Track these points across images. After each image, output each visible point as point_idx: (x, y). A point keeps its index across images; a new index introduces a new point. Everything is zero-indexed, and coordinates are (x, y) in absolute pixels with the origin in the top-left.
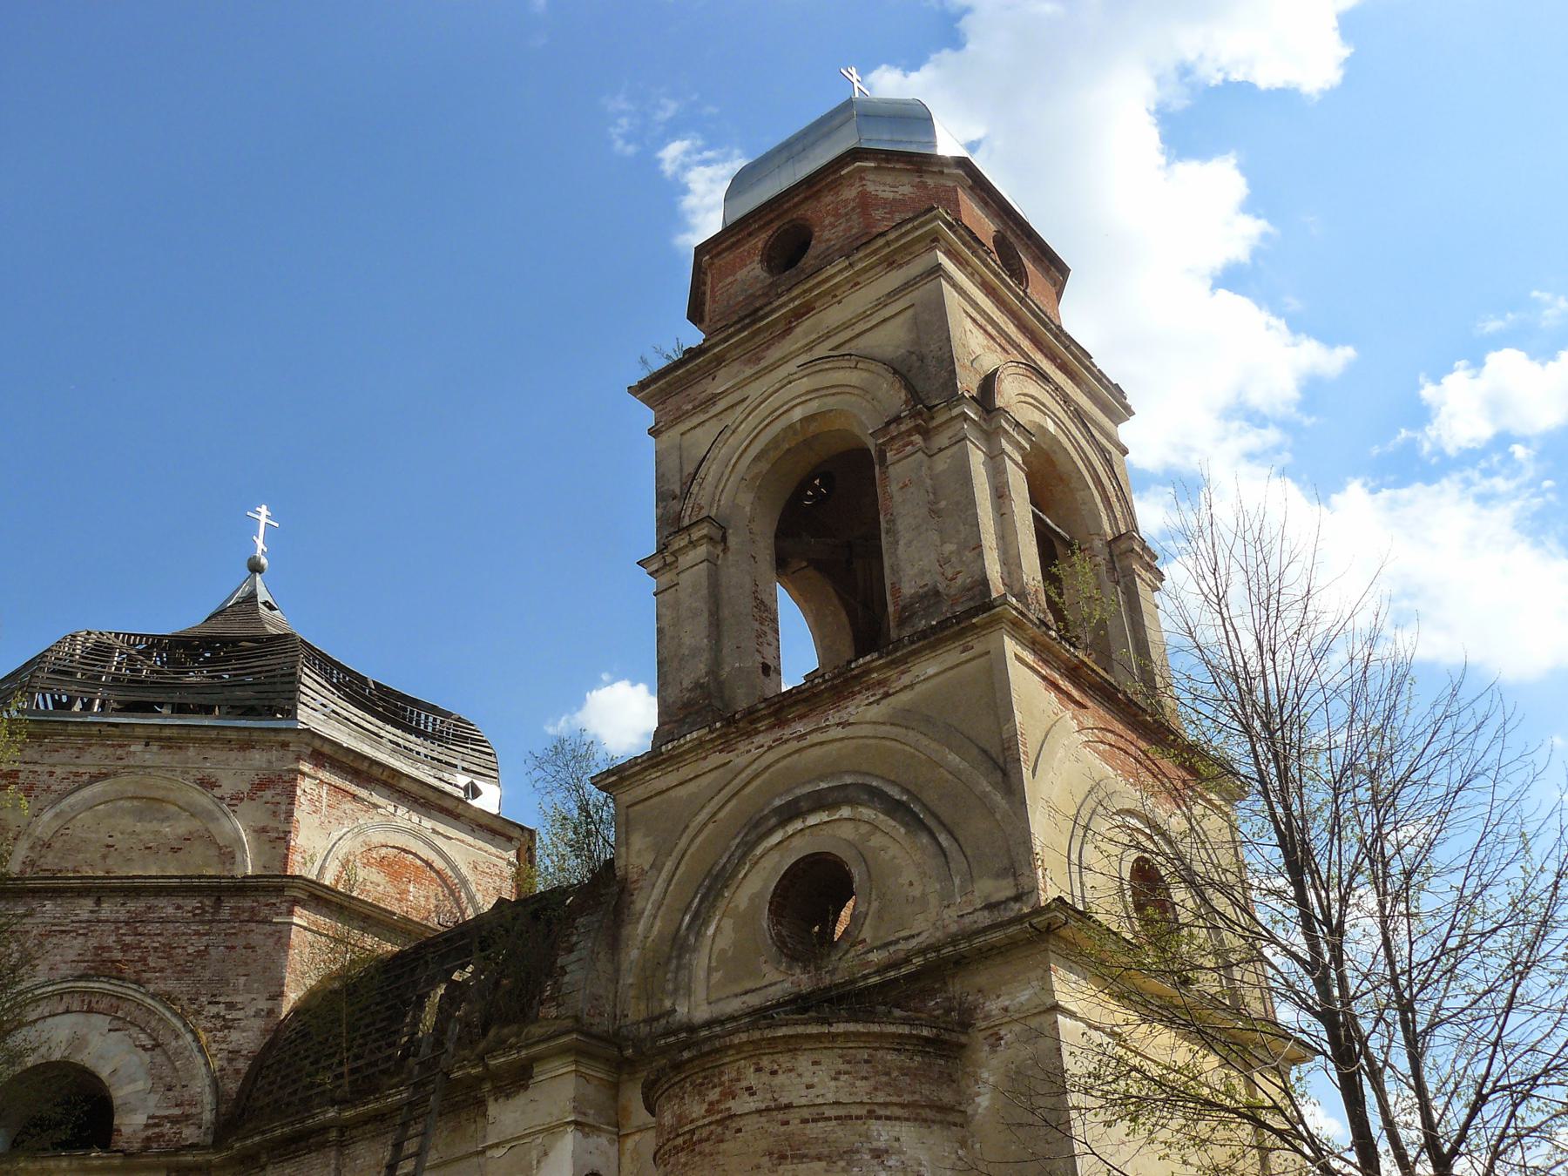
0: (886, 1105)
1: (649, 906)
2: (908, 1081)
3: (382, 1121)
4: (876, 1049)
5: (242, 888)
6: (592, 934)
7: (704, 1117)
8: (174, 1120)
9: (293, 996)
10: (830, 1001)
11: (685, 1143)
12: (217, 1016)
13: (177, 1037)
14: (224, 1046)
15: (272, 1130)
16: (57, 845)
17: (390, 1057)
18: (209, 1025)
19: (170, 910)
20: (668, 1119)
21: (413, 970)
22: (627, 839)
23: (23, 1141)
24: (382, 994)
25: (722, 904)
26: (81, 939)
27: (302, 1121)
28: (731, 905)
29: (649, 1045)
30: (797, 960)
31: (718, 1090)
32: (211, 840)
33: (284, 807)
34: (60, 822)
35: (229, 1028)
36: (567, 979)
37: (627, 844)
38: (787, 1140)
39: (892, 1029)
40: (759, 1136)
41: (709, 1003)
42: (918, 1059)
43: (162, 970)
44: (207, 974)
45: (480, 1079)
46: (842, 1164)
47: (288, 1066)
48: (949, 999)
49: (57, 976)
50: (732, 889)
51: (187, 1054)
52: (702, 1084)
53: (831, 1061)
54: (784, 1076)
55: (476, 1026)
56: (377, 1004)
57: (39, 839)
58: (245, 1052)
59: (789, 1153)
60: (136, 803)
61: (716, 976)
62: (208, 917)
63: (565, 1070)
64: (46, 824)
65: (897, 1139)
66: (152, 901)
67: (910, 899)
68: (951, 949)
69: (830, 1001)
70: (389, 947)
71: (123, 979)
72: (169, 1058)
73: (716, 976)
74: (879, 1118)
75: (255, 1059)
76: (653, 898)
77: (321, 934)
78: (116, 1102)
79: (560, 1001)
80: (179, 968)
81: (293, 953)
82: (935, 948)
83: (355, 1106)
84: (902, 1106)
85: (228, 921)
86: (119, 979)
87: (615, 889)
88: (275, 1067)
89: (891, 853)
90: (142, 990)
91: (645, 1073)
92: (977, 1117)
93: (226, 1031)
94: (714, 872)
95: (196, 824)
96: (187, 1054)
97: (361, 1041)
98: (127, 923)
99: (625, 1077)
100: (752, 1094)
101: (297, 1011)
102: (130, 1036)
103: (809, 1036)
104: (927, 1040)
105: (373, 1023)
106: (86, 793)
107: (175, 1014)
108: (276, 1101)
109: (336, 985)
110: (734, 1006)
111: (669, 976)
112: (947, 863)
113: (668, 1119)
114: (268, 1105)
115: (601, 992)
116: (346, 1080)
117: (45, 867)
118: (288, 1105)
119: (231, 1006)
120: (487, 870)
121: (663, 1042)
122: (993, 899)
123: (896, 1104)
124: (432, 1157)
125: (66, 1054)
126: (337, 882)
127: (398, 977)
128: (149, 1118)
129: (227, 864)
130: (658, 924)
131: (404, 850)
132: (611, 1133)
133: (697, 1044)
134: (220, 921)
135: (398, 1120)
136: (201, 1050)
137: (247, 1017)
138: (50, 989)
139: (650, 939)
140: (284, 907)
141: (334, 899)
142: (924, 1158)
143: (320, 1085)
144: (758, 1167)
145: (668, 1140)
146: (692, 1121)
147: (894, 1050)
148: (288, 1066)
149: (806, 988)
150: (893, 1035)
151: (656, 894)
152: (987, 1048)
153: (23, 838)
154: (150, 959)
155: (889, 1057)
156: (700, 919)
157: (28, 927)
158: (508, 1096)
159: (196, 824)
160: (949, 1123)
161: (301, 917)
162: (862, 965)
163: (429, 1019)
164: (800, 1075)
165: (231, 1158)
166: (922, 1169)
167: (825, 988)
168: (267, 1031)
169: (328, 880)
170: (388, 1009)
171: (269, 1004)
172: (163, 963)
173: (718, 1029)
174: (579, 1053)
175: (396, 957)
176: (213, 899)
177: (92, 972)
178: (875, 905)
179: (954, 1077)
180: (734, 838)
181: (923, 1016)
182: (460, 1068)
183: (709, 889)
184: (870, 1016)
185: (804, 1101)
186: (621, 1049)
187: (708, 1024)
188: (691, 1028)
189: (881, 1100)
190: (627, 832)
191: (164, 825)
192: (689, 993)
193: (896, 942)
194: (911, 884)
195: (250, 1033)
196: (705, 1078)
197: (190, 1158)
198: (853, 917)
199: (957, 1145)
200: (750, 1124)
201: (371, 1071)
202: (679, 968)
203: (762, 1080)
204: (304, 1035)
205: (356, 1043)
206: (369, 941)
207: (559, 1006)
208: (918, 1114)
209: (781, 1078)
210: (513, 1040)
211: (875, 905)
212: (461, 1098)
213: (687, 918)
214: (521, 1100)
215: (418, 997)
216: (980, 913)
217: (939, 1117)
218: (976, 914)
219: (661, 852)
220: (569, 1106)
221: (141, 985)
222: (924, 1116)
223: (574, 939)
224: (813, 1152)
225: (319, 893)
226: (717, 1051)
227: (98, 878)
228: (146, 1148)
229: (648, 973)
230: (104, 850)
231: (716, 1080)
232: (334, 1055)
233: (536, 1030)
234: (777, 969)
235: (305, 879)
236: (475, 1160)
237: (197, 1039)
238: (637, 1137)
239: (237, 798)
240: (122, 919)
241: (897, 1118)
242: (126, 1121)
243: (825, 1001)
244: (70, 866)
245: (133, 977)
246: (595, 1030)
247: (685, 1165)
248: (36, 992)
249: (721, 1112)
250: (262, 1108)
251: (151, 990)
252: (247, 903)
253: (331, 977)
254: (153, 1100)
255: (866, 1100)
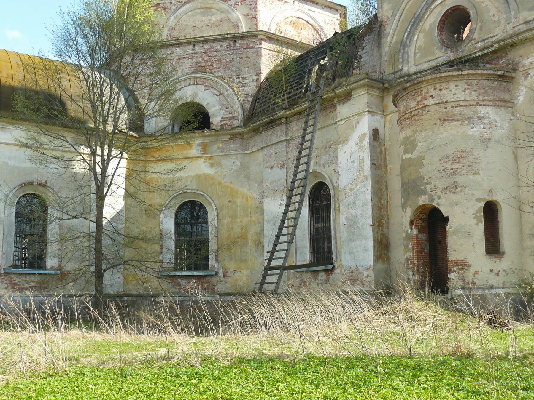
0: (483, 100)
1: (391, 31)
2: (492, 91)
3: (300, 114)
4: (480, 80)
5: (242, 37)
6: (371, 43)
7: (415, 107)
8: (230, 119)
9: (265, 73)
10: (462, 63)
11: (408, 116)
12: (240, 82)
13: (227, 90)
14: (243, 92)
15: (263, 120)
16: (177, 28)
17: (301, 92)
18: (237, 86)
19: (219, 47)
20: (402, 108)
21: (306, 61)
22: (382, 6)
23: (183, 128)
24: (296, 70)
25: (419, 28)
26: (190, 60)
27: (273, 116)
28: (423, 28)
29: (394, 82)
30: (449, 48)
31: (420, 97)
32: (229, 20)
33: (253, 6)
34: (177, 20)
35: (244, 86)
36: (362, 59)
37: (382, 8)
38: (446, 114)
39: (486, 72)
40: (436, 113)
41: (416, 66)
42: (496, 83)
43: (219, 68)
44: (234, 68)
45: (334, 98)
46: (467, 122)
47: (266, 98)
48: (508, 60)
49: (184, 73)
50: (423, 22)
51: (231, 96)
52: (414, 95)
53: (462, 85)
54: (445, 91)
55: (331, 79)
56: (295, 74)
57: (171, 27)
58: (251, 94)
59: (447, 119)
60: (201, 10)
61: (418, 55)
62: (232, 48)
63: (363, 93)
64: (172, 21)
65: (488, 113)
66: (212, 44)
67: (493, 22)
68: (510, 40)
69: (462, 63)
70: (297, 54)
71: (207, 73)
72: (225, 98)
73: (418, 55)
74: (480, 105)
75: (254, 96)
76: (393, 27)
77: (272, 51)
78: (210, 114)
79: (360, 68)
80: (225, 67)
81: (263, 58)
82: (504, 40)
83: (290, 110)
84: (490, 101)
85: (239, 49)
86: (205, 72)
87: (378, 25)
88: (261, 98)
89: (486, 3)
90: (213, 76)
91: (393, 92)
92: (518, 104)
93: (243, 87)
94: (416, 16)
95: (223, 16)
96: (231, 96)
97: (290, 87)
98: (205, 53)
99: (385, 94)
100: (433, 98)
101: (267, 79)
102: (211, 92)
103: (454, 76)
104: (500, 76)
105: (294, 81)
106: (184, 8)
107: (225, 83)
108: (263, 110)
109: (279, 68)
110: (425, 66)
111: (400, 56)
112: (509, 6)
113: (402, 108)
114: (260, 111)
115: (375, 64)
116: (286, 101)
117: (174, 36)
118: (267, 111)
119: (244, 79)
120: (329, 23)
121: (399, 81)
122: (527, 20)
123: (487, 100)
124: (318, 126)
125: (192, 99)
126: (276, 31)
127: (301, 64)
128: (221, 118)
129: (236, 28)
130: (395, 37)
131: (298, 18)
132: (381, 114)
133: (412, 80)
134: (236, 49)
135: (306, 114)
136: (235, 94)
137: (249, 82)
138: (183, 78)
139: (393, 43)
140: (258, 42)
141: (275, 38)
142: (498, 120)
143: (277, 103)
144: (436, 124)
145: (402, 116)
146: (411, 109)
147: (487, 80)
148: (266, 98)
149: (452, 59)
150: (487, 74)
151: (394, 26)
152: (523, 78)
153: (165, 27)
154: (214, 64)
155: (484, 83)
156: (411, 34)
157: (172, 58)
158: (343, 103)
159: (223, 16)
160: (507, 107)
161: (264, 45)
162: (474, 48)
163: (313, 77)
164: (451, 90)
165: (250, 130)
166: (497, 124)
167: (460, 58)
168: (257, 86)
169: (272, 31)
170: (298, 75)
171: (257, 77)
172: (219, 66)
173: (419, 75)
174: (369, 86)
175: (299, 57)
176: (233, 41)
177: (196, 71)
178: (479, 25)
179: (510, 90)
180: (423, 2)
181: (498, 66)
182: (326, 94)
183: (414, 22)
184: (477, 67)
185: (452, 100)
186: (383, 84)
187: (416, 73)
188: (409, 75)
189: (482, 99)
190: (381, 3)
191: (212, 17)
192: (408, 62)
193: (488, 39)
194: (494, 15)
195: (251, 87)
196: (415, 93)
197: (236, 131)
198: (471, 30)
199: (510, 115)
200: (432, 109)
201: (294, 97)
202: (403, 53)
203: (437, 93)
204: (270, 86)
205: (288, 88)
206: (289, 51)
207: (360, 70)
208: (495, 103)
209: (444, 91)
210: (344, 83)
211: (479, 25)
212: (328, 104)
213: (406, 34)
214: (348, 104)
215: (309, 70)
216: (522, 25)
217: (504, 104)
218: (521, 26)
219: (395, 10)
220: (366, 106)
221: (212, 74)
222: (498, 104)
223: (364, 45)
224: (456, 118)
225: (270, 36)
226: (419, 83)
227: (192, 38)
228: (222, 128)
229: (392, 56)
230: (193, 28)
231: (419, 93)
232: (281, 93)
233: (352, 79)
234: (441, 51)
235: (264, 31)
236: (333, 126)
237: (234, 91)
238: (391, 115)
239: (236, 4)
240: (203, 52)
241: (488, 105)
242: (214, 120)
243: (460, 63)
244: (183, 35)
245: (210, 71)
246: (373, 78)
247: (409, 124)
248: (179, 79)
249: (421, 105)
250: (258, 113)
251: (216, 75)
252: (245, 42)
253: (277, 66)
254: (222, 112)
255: (476, 99)
